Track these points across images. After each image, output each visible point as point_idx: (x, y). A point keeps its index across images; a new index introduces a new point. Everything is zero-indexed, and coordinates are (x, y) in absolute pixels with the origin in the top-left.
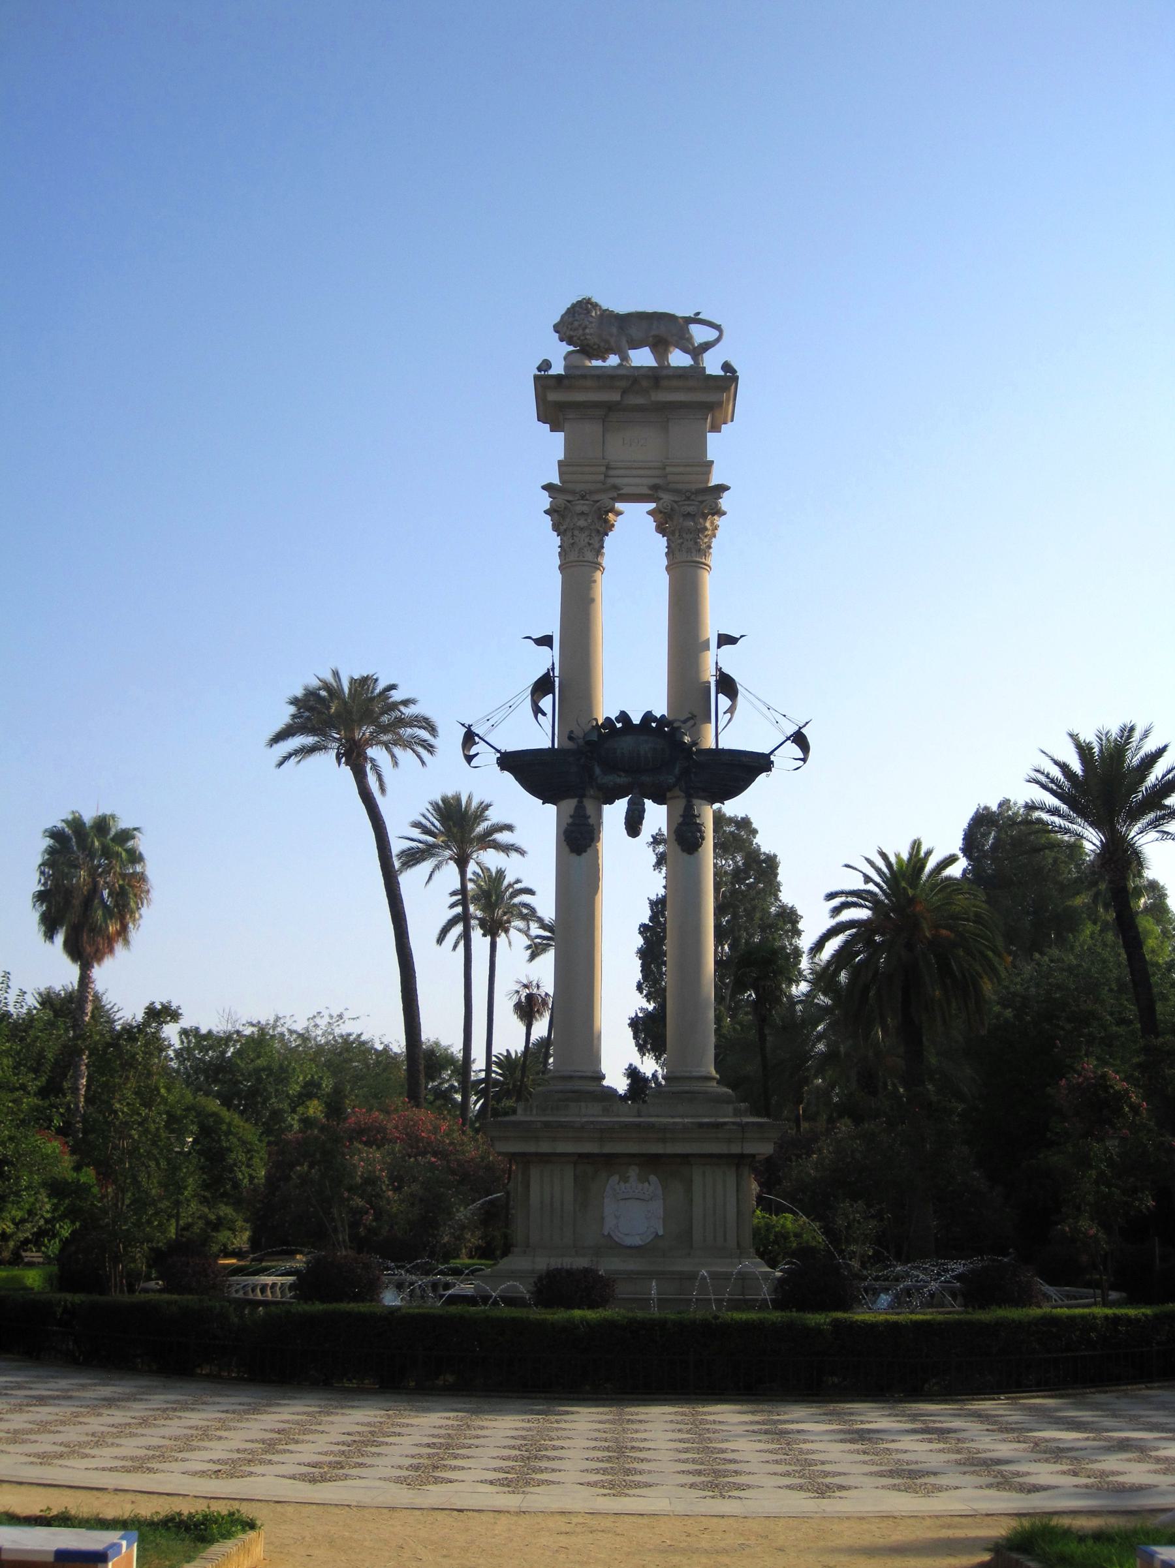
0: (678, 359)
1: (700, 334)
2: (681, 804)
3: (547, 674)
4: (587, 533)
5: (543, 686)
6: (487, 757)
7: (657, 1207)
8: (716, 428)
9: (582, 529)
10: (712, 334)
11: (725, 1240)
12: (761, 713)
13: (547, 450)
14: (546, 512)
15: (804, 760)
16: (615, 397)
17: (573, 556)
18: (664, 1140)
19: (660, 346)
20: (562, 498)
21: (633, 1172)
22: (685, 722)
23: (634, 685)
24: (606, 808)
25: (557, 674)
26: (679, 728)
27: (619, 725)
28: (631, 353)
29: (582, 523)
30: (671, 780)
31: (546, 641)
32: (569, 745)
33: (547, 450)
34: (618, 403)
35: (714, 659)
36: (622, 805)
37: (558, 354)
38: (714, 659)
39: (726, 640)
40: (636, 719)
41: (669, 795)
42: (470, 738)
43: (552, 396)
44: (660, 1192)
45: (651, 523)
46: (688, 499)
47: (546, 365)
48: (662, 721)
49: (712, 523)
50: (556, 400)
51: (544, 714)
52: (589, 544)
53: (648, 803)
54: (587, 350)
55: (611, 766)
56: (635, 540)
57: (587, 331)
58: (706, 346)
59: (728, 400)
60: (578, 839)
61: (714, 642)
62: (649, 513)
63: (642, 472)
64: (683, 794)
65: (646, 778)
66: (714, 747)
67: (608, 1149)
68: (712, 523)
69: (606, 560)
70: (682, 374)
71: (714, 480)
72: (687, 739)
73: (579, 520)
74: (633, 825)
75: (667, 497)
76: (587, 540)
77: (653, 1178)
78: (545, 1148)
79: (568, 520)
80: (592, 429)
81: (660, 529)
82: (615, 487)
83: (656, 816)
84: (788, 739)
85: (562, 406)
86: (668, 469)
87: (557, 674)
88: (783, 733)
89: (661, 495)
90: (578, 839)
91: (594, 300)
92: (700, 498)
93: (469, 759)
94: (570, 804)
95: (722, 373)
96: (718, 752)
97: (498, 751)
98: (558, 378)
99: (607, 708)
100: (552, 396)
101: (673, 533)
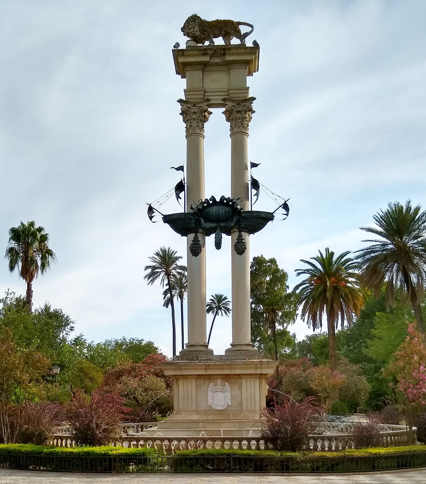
0: (235, 41)
1: (243, 29)
2: (236, 235)
3: (182, 181)
4: (197, 121)
5: (180, 187)
6: (158, 217)
7: (228, 395)
8: (250, 74)
9: (194, 119)
10: (249, 29)
11: (255, 407)
12: (269, 196)
13: (178, 86)
14: (180, 114)
15: (287, 215)
16: (206, 59)
17: (191, 131)
18: (230, 369)
19: (227, 36)
20: (186, 106)
21: (219, 381)
22: (238, 199)
23: (217, 185)
24: (207, 238)
25: (186, 182)
26: (235, 202)
27: (211, 202)
28: (214, 40)
29: (194, 116)
30: (233, 224)
31: (181, 168)
32: (191, 211)
33: (178, 86)
34: (208, 62)
35: (252, 173)
36: (213, 236)
37: (183, 41)
38: (252, 173)
39: (254, 165)
40: (218, 200)
41: (232, 231)
42: (151, 210)
43: (181, 60)
44: (229, 389)
45: (224, 117)
46: (239, 104)
47: (177, 45)
48: (228, 200)
49: (249, 116)
50: (183, 63)
51: (180, 198)
52: (198, 126)
53: (224, 235)
54: (195, 39)
55: (208, 219)
56: (217, 122)
57: (195, 29)
58: (246, 35)
59: (256, 58)
60: (195, 250)
61: (249, 166)
62: (223, 113)
63: (220, 94)
64: (237, 230)
65: (222, 224)
66: (250, 210)
67: (209, 372)
68: (249, 116)
69: (215, 19)
70: (236, 47)
71: (250, 96)
72: (239, 207)
73: (194, 113)
74: (218, 245)
75: (229, 104)
76: (196, 124)
77: (227, 384)
78: (185, 373)
79: (189, 116)
80: (198, 74)
81: (228, 120)
82: (209, 100)
83: (227, 240)
84: (280, 206)
85: (185, 65)
86: (230, 92)
87: (186, 182)
88: (278, 203)
89: (227, 103)
90: (195, 250)
91: (198, 15)
92: (244, 104)
93: (151, 218)
94: (192, 236)
95: (253, 46)
96: (252, 212)
97: (163, 215)
98: (182, 50)
99: (207, 195)
100: (181, 60)
101: (232, 120)
